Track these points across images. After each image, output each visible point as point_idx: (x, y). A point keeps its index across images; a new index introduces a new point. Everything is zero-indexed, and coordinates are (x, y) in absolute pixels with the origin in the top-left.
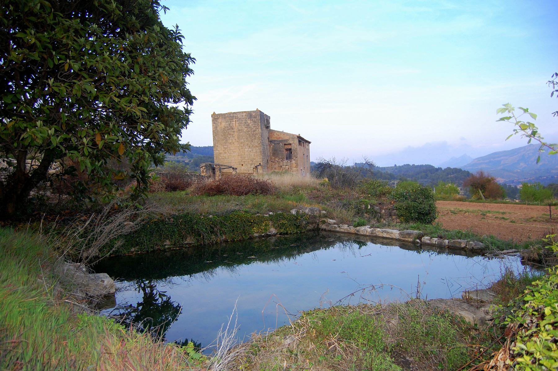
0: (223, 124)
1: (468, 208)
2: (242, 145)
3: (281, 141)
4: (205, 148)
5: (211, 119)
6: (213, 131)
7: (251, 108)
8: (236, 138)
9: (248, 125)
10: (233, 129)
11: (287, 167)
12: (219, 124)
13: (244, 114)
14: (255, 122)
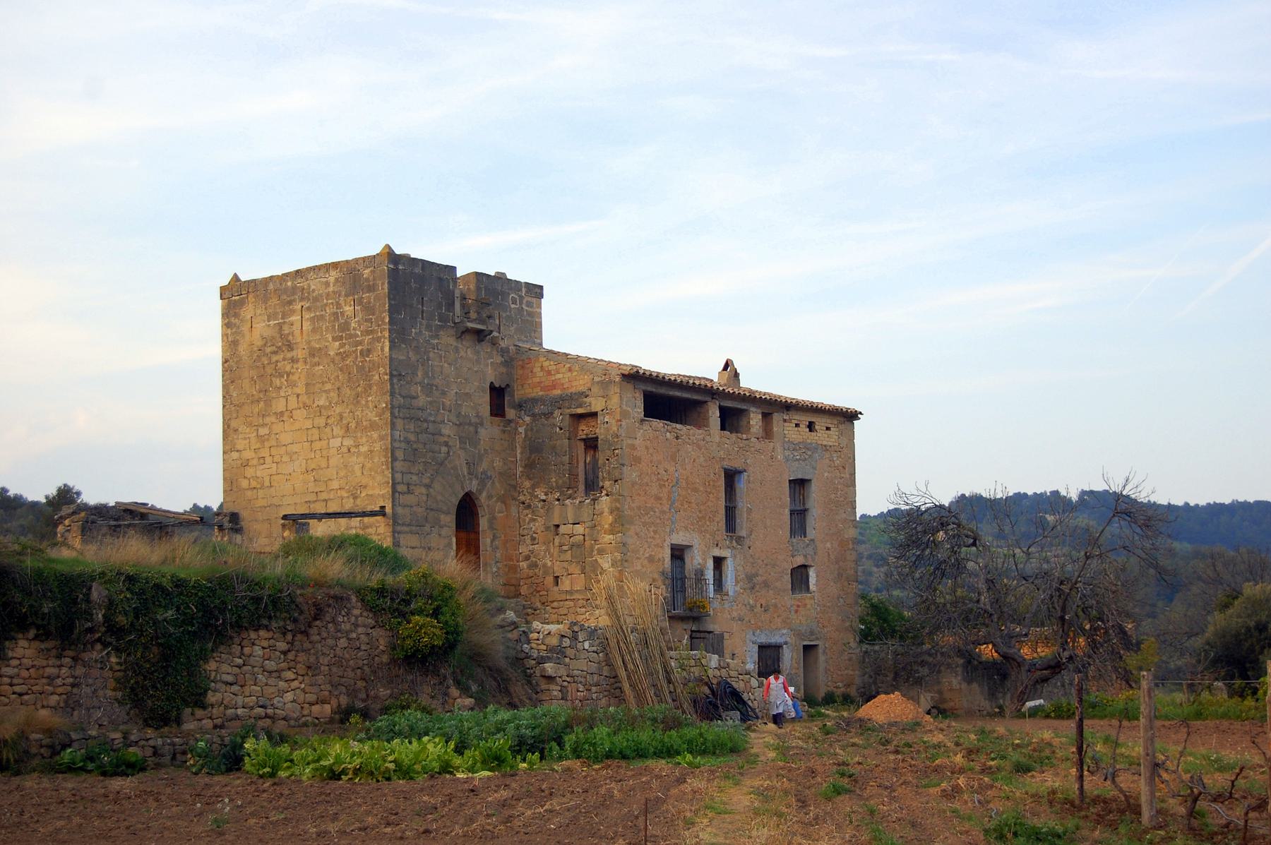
0: (259, 327)
1: (1168, 699)
2: (321, 421)
3: (559, 402)
4: (1216, 510)
5: (217, 305)
6: (225, 361)
7: (359, 243)
8: (300, 389)
9: (345, 327)
10: (290, 347)
11: (579, 529)
12: (245, 328)
13: (334, 275)
14: (368, 309)
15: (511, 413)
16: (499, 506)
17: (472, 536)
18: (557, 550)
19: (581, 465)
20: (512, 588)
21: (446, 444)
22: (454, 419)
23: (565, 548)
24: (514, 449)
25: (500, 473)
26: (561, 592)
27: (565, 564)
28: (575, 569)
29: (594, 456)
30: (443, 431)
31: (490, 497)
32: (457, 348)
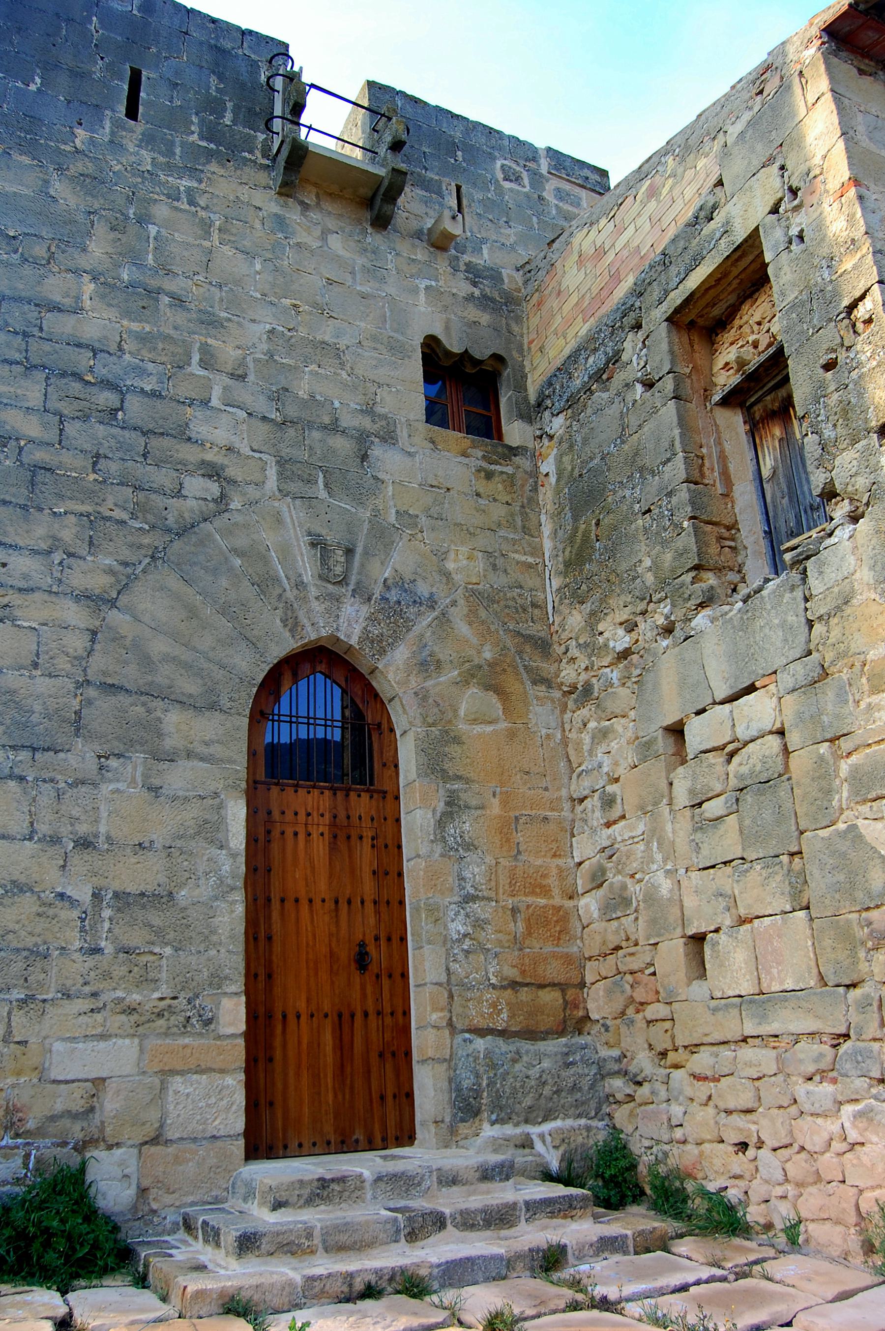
11: (759, 710)
15: (515, 432)
16: (471, 699)
17: (362, 804)
18: (685, 822)
19: (745, 495)
20: (550, 998)
21: (213, 472)
22: (262, 406)
23: (713, 808)
24: (530, 530)
25: (473, 594)
26: (721, 1003)
27: (722, 878)
28: (762, 890)
29: (787, 441)
30: (200, 429)
31: (427, 665)
32: (280, 222)
